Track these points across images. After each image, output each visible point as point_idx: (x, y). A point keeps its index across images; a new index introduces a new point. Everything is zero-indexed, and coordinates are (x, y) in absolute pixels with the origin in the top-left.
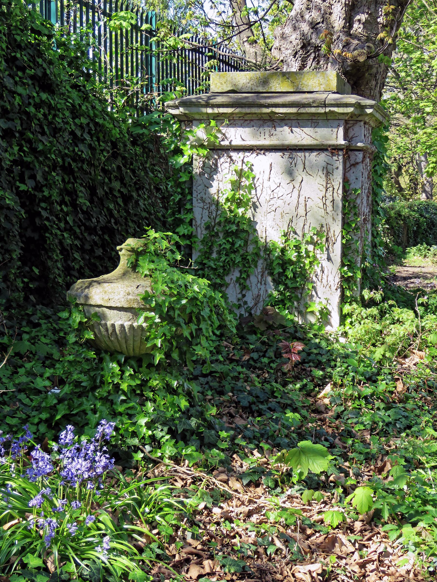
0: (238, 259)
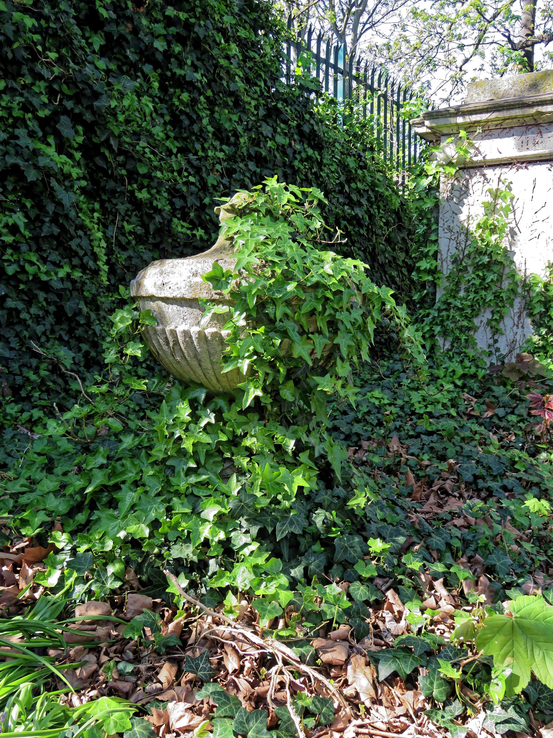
0: (490, 297)
